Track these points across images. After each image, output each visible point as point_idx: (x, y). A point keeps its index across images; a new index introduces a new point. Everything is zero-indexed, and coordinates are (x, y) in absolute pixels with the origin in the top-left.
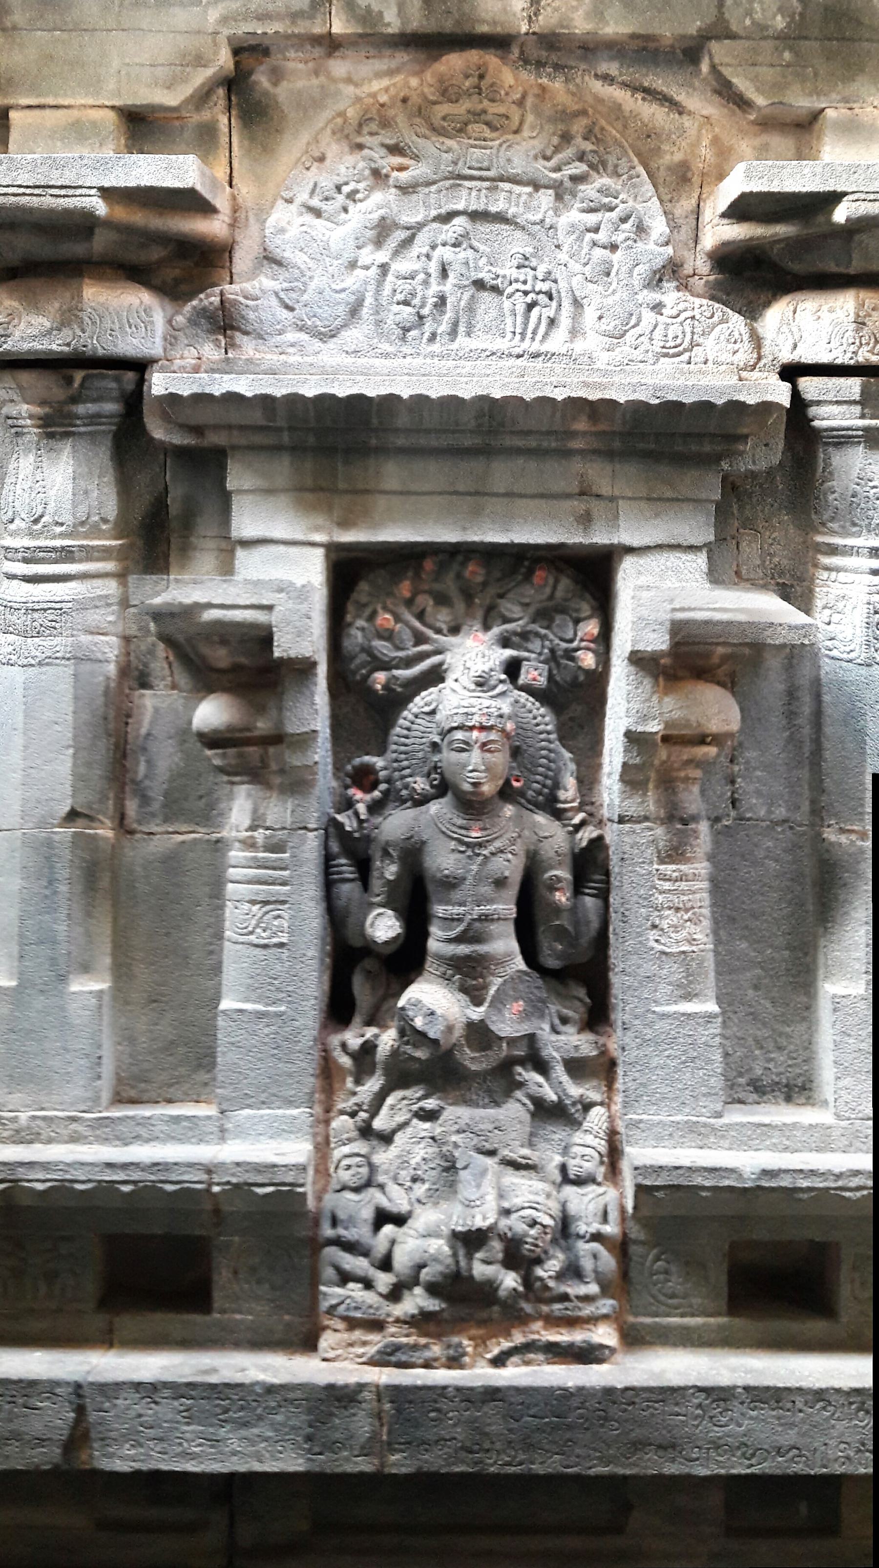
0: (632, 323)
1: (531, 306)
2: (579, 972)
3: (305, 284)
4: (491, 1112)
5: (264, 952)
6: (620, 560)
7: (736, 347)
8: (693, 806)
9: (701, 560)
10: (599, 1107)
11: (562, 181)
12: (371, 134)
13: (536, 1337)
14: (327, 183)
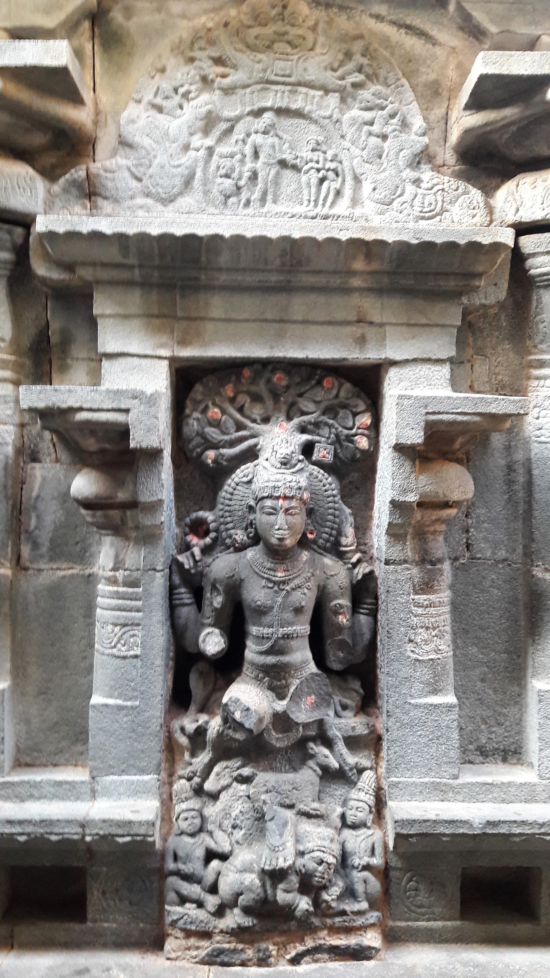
0: (398, 193)
1: (322, 180)
2: (355, 671)
3: (150, 161)
4: (291, 776)
5: (122, 661)
6: (386, 372)
7: (475, 212)
8: (439, 552)
9: (445, 370)
10: (369, 771)
11: (345, 86)
12: (201, 49)
13: (322, 942)
14: (166, 86)
